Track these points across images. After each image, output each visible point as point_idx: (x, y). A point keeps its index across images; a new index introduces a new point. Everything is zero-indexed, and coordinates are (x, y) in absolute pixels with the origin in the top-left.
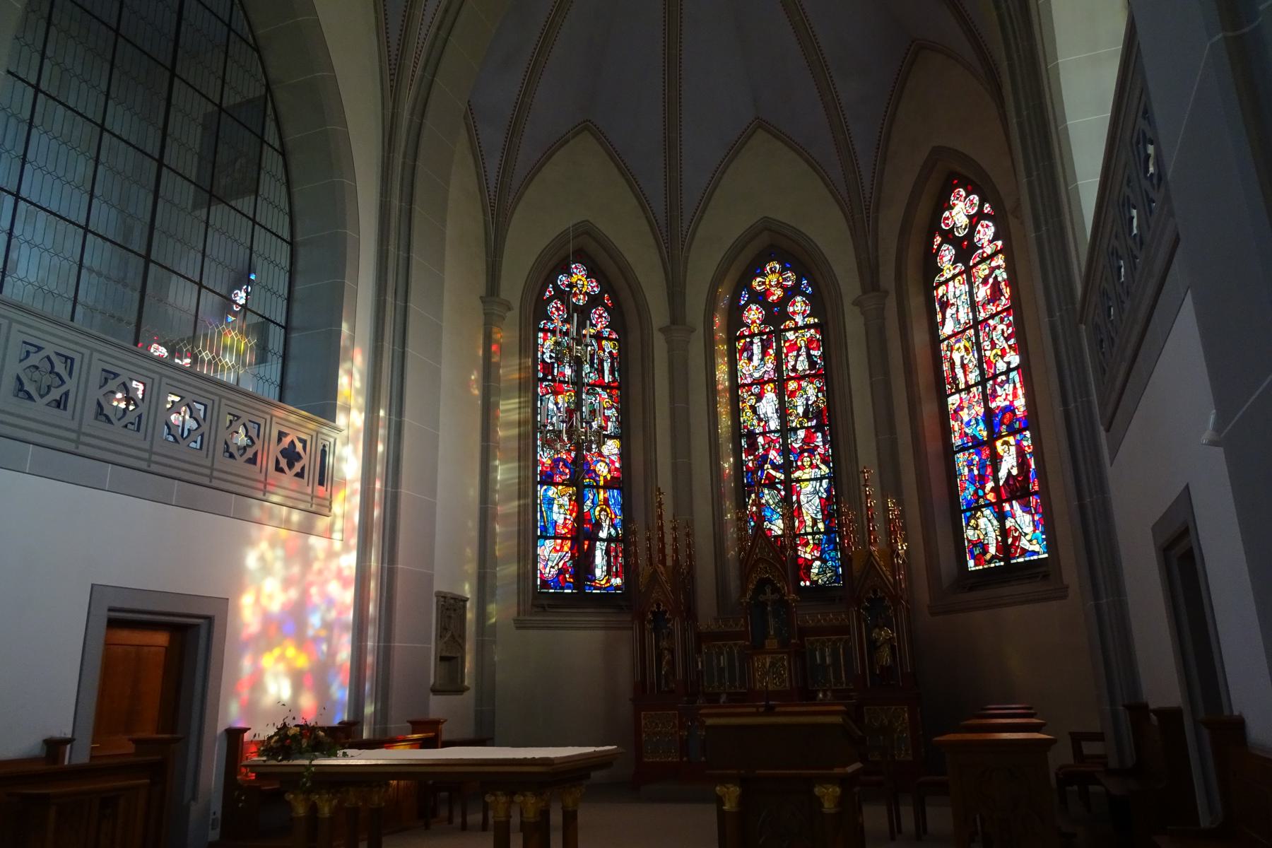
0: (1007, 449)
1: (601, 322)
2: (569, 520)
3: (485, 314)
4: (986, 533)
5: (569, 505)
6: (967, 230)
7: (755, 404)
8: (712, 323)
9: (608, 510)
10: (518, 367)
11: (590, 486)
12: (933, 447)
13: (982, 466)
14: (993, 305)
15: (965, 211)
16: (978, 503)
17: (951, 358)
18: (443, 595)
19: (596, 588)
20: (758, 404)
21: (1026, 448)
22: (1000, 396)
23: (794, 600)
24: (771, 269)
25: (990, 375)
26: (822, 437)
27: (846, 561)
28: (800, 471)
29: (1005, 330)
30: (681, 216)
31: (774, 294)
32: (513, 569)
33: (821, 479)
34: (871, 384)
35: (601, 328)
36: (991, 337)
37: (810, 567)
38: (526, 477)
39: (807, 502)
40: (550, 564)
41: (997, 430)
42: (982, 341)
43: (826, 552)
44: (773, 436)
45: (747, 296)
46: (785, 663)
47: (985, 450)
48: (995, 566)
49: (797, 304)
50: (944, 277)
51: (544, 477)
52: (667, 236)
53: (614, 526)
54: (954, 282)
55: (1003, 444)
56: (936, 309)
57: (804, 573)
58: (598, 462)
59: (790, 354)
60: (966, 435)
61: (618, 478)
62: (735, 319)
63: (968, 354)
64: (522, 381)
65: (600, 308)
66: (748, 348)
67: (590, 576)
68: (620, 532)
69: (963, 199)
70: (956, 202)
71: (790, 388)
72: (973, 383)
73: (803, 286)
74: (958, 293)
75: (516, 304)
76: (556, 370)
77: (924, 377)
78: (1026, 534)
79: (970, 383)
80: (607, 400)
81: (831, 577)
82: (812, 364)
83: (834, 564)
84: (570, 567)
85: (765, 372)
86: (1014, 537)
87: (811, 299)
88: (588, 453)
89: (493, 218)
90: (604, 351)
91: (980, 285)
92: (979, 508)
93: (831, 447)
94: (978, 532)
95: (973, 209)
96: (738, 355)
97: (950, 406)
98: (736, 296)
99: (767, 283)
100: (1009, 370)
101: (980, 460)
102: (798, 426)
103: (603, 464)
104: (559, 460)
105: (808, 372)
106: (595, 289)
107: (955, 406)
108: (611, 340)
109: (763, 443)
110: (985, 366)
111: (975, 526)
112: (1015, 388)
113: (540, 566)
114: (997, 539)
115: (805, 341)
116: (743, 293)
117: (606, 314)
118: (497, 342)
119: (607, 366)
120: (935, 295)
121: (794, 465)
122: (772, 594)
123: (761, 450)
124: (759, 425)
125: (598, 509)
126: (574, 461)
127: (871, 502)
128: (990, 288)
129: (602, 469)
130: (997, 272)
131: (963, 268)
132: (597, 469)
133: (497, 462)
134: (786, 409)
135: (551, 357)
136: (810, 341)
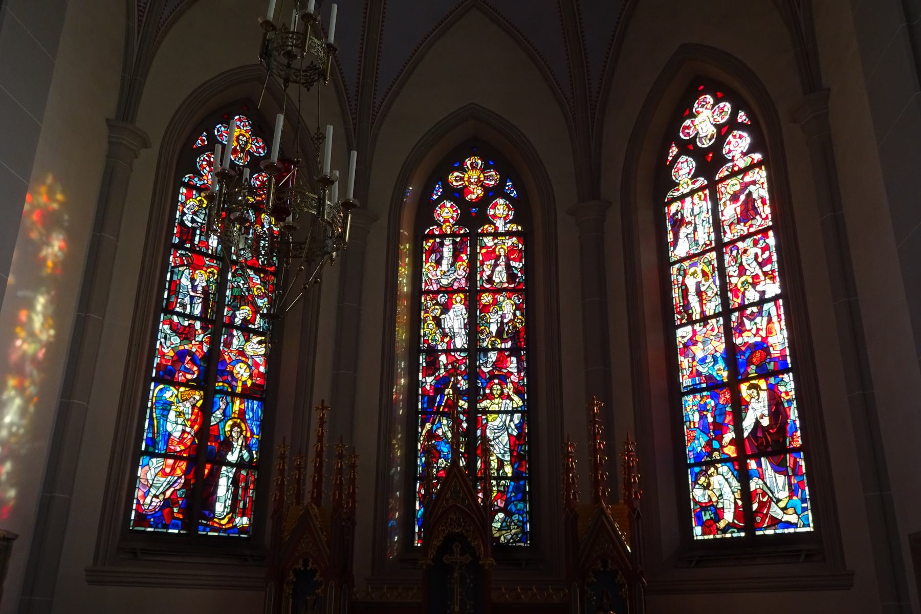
2: (189, 433)
3: (109, 142)
4: (721, 495)
5: (192, 414)
6: (713, 140)
7: (440, 315)
9: (243, 425)
11: (222, 392)
13: (718, 412)
14: (744, 226)
15: (712, 120)
17: (683, 283)
19: (213, 529)
20: (444, 316)
21: (783, 395)
22: (750, 331)
24: (472, 164)
25: (737, 305)
26: (517, 363)
29: (760, 253)
30: (376, 86)
31: (473, 193)
33: (512, 412)
36: (739, 261)
37: (492, 519)
40: (153, 491)
41: (742, 370)
42: (726, 266)
43: (513, 502)
45: (441, 190)
47: (724, 393)
48: (732, 537)
49: (498, 206)
50: (680, 192)
51: (161, 373)
53: (248, 447)
55: (749, 388)
58: (238, 361)
60: (699, 374)
63: (706, 280)
65: (263, 174)
66: (437, 250)
67: (207, 513)
68: (255, 456)
69: (709, 106)
70: (700, 110)
71: (483, 302)
72: (712, 313)
73: (507, 188)
74: (696, 211)
76: (197, 239)
78: (779, 500)
79: (708, 313)
80: (260, 286)
81: (515, 534)
82: (511, 277)
83: (521, 518)
84: (181, 497)
87: (514, 203)
88: (226, 349)
89: (139, 26)
91: (728, 202)
92: (713, 463)
93: (527, 375)
94: (710, 492)
95: (722, 118)
96: (424, 256)
97: (679, 339)
98: (429, 190)
99: (466, 179)
100: (762, 301)
101: (716, 405)
102: (490, 347)
103: (244, 366)
105: (506, 285)
107: (686, 340)
109: (445, 362)
110: (730, 295)
111: (705, 484)
112: (770, 321)
113: (139, 493)
114: (736, 503)
115: (505, 250)
116: (437, 186)
120: (666, 211)
121: (482, 393)
123: (442, 371)
124: (442, 341)
125: (230, 422)
126: (207, 357)
129: (242, 372)
132: (235, 371)
134: (478, 325)
135: (193, 221)
136: (511, 250)
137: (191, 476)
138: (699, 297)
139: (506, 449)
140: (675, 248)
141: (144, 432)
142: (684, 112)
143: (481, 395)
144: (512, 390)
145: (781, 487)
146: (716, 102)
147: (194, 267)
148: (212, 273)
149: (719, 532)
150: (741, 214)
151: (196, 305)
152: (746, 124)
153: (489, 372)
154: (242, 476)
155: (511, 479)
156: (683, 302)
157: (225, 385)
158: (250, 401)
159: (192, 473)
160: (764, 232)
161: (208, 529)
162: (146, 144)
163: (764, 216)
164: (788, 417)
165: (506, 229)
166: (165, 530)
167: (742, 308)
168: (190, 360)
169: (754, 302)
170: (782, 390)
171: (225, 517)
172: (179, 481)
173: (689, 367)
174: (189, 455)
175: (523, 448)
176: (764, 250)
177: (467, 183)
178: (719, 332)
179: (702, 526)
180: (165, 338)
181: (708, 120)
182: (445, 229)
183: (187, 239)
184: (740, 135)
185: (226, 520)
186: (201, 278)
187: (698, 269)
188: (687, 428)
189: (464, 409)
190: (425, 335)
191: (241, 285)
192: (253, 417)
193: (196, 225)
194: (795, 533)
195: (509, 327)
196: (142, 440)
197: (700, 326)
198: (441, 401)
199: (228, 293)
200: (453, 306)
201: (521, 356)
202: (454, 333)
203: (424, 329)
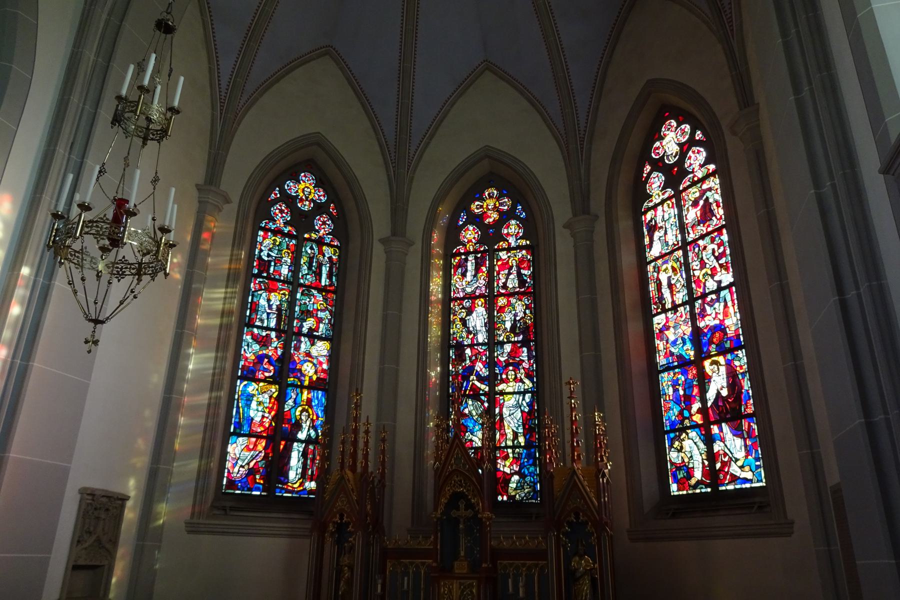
0: (716, 369)
1: (324, 228)
2: (267, 418)
3: (199, 202)
4: (691, 457)
5: (270, 403)
6: (678, 157)
7: (466, 317)
8: (430, 238)
9: (310, 410)
10: (228, 258)
11: (293, 385)
12: (637, 364)
13: (688, 386)
14: (704, 226)
15: (676, 140)
16: (683, 425)
17: (658, 279)
18: (88, 492)
19: (288, 491)
20: (468, 317)
21: (738, 369)
22: (710, 315)
23: (489, 519)
24: (489, 194)
25: (699, 294)
26: (528, 352)
27: (546, 477)
28: (505, 384)
29: (716, 249)
31: (490, 217)
32: (194, 464)
34: (578, 302)
35: (324, 234)
38: (223, 370)
39: (510, 415)
40: (240, 463)
41: (705, 349)
42: (690, 262)
44: (481, 349)
45: (465, 217)
46: (474, 591)
47: (692, 369)
48: (701, 492)
49: (511, 226)
50: (653, 202)
51: (245, 372)
52: (395, 156)
53: (315, 428)
54: (663, 206)
56: (644, 233)
57: (501, 487)
58: (305, 361)
59: (502, 272)
60: (672, 354)
61: (324, 380)
62: (452, 237)
63: (675, 275)
64: (231, 271)
65: (324, 216)
66: (463, 265)
67: (282, 479)
68: (320, 434)
69: (673, 129)
70: (667, 133)
71: (500, 304)
72: (680, 302)
74: (666, 217)
75: (235, 198)
77: (630, 296)
78: (737, 460)
79: (677, 303)
80: (322, 302)
82: (522, 282)
84: (262, 467)
85: (477, 288)
86: (722, 462)
87: (524, 223)
88: (296, 352)
90: (324, 256)
91: (690, 208)
92: (684, 430)
93: (536, 362)
94: (683, 455)
95: (684, 138)
96: (453, 270)
97: (655, 326)
98: (455, 217)
99: (485, 207)
100: (720, 289)
101: (686, 380)
102: (505, 340)
103: (310, 365)
104: (266, 356)
105: (518, 289)
106: (322, 198)
107: (661, 326)
108: (332, 246)
109: (470, 354)
110: (694, 285)
111: (679, 448)
112: (726, 306)
113: (229, 465)
114: (703, 463)
116: (462, 214)
117: (330, 222)
118: (209, 230)
119: (325, 270)
120: (643, 219)
122: (466, 509)
123: (468, 362)
124: (467, 337)
125: (300, 409)
126: (281, 359)
127: (575, 415)
128: (701, 210)
129: (309, 369)
130: (708, 194)
131: (673, 193)
133: (192, 351)
134: (495, 323)
135: (269, 256)
136: (521, 261)
137: (269, 451)
138: (670, 289)
139: (519, 423)
140: (650, 250)
141: (232, 418)
142: (655, 135)
143: (499, 380)
144: (523, 375)
145: (738, 448)
146: (679, 125)
147: (269, 290)
148: (284, 294)
149: (691, 488)
150: (701, 216)
151: (272, 320)
152: (702, 141)
153: (505, 361)
154: (310, 450)
155: (523, 447)
156: (658, 294)
157: (296, 380)
158: (316, 392)
159: (271, 447)
160: (719, 230)
161: (284, 491)
162: (227, 201)
163: (718, 217)
164: (742, 387)
165: (517, 244)
166: (249, 493)
167: (704, 296)
168: (268, 362)
169: (713, 291)
170: (737, 365)
171: (297, 482)
172: (260, 454)
173: (664, 349)
174: (268, 434)
175: (533, 422)
176: (719, 246)
177: (485, 210)
178: (686, 318)
179: (677, 483)
180: (248, 345)
181: (673, 141)
182: (469, 248)
183: (264, 269)
184: (698, 150)
185: (298, 484)
186: (275, 299)
187: (669, 266)
188: (664, 401)
189: (486, 392)
190: (454, 333)
191: (307, 302)
192: (318, 404)
193: (270, 259)
194: (751, 488)
195: (521, 323)
196: (231, 424)
197: (672, 314)
198: (467, 386)
199: (297, 309)
200: (476, 309)
201: (531, 346)
202: (477, 330)
203: (453, 328)
